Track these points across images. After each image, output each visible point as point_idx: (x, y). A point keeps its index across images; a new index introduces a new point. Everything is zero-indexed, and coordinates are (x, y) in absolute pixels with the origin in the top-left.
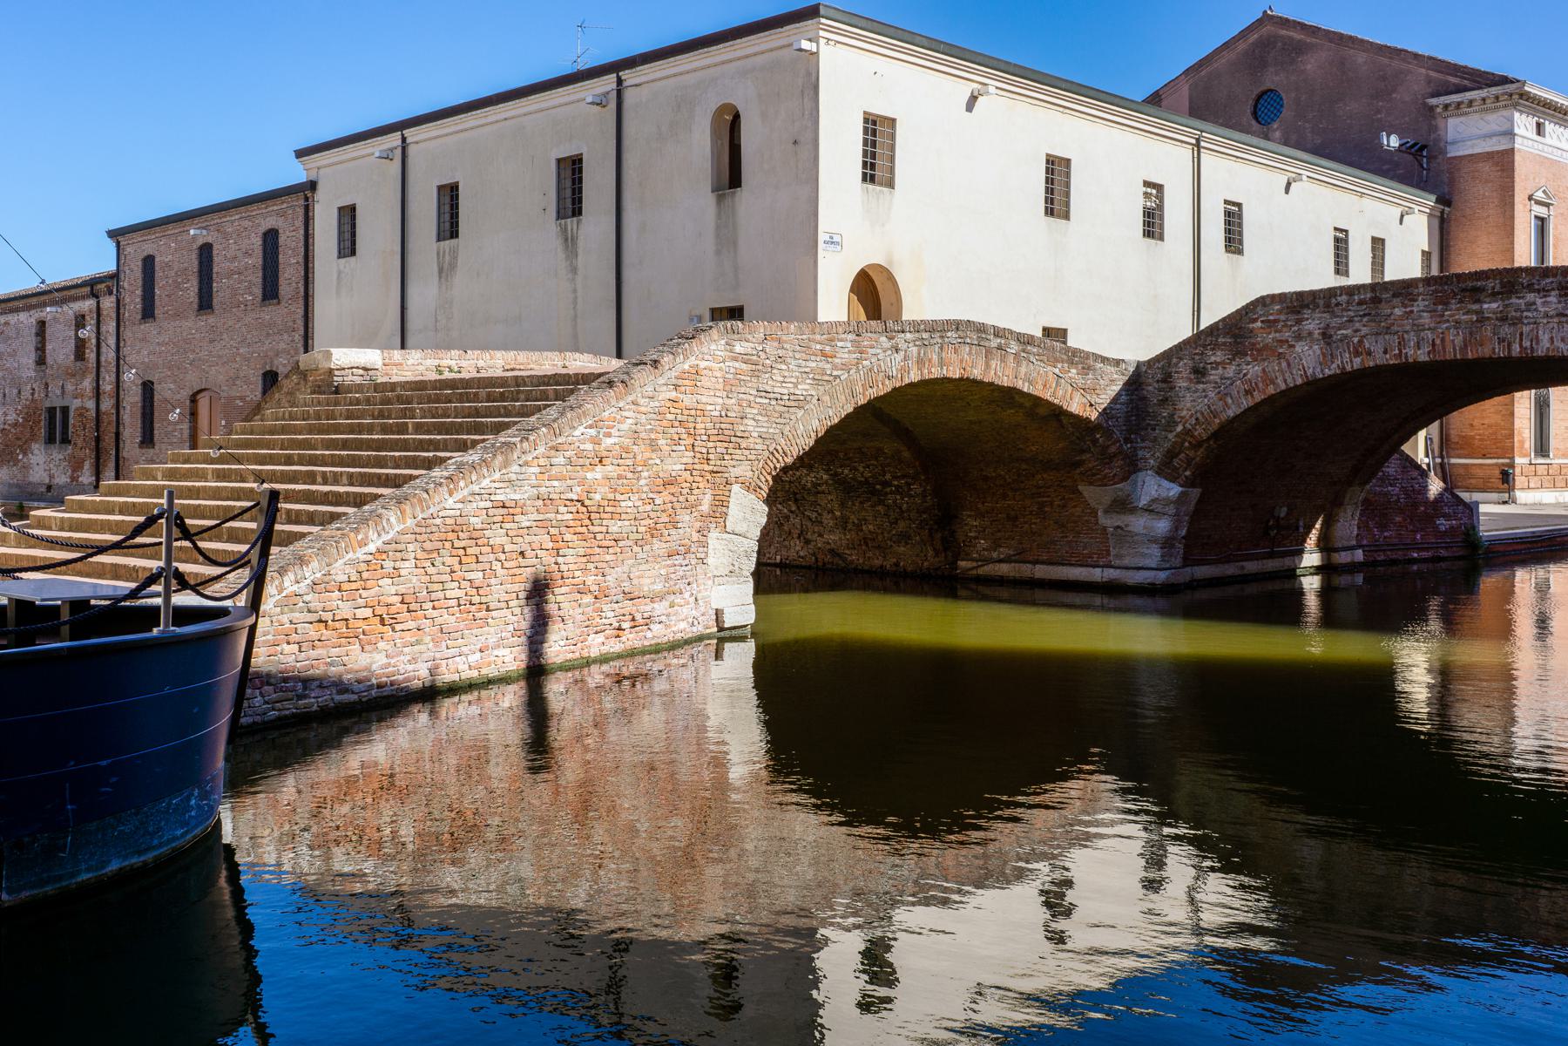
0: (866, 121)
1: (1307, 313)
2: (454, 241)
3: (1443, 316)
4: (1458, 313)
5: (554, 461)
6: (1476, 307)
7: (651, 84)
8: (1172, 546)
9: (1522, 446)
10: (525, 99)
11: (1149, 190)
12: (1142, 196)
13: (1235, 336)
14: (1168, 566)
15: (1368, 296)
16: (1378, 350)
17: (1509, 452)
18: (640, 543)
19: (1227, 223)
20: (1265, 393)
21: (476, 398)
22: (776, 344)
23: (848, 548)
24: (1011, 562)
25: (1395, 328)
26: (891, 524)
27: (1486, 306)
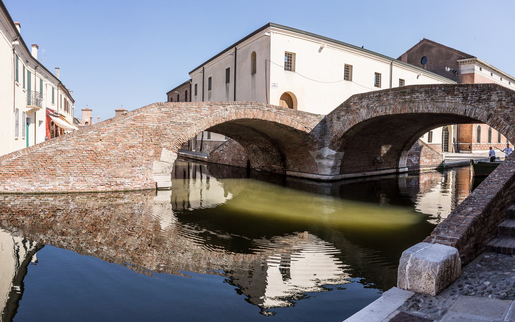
6: (404, 97)
9: (474, 141)
13: (347, 107)
14: (334, 174)
16: (380, 110)
17: (471, 141)
20: (353, 124)
25: (384, 104)
27: (406, 97)
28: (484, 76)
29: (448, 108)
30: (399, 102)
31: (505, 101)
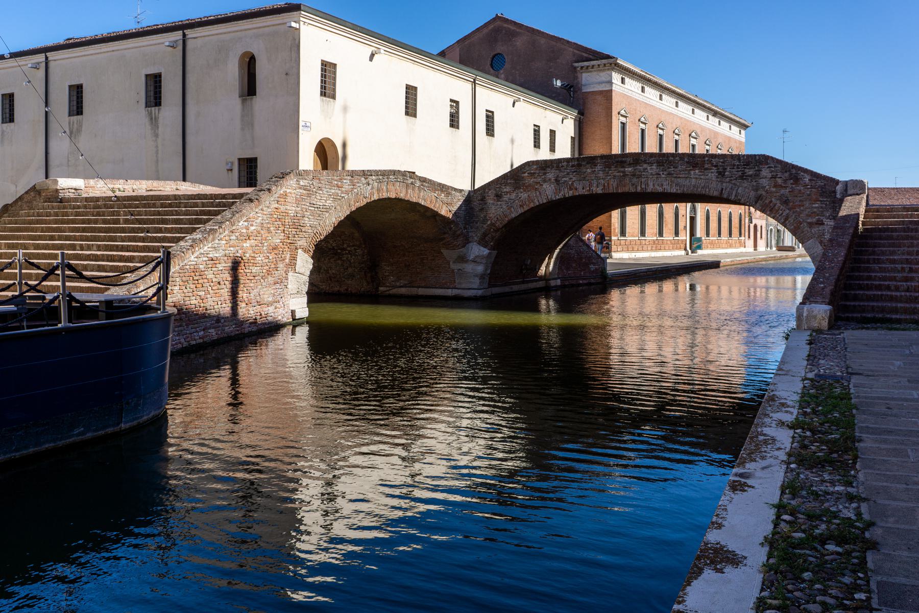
0: (322, 64)
1: (548, 170)
2: (79, 117)
3: (608, 173)
4: (614, 172)
5: (232, 238)
6: (622, 169)
7: (203, 38)
8: (484, 278)
10: (126, 41)
11: (452, 104)
12: (449, 106)
13: (515, 180)
15: (576, 163)
16: (580, 187)
18: (263, 278)
19: (487, 121)
21: (154, 206)
22: (318, 181)
23: (321, 282)
24: (406, 287)
25: (587, 178)
26: (345, 269)
27: (626, 169)
28: (629, 94)
29: (694, 186)
30: (614, 176)
31: (781, 178)
